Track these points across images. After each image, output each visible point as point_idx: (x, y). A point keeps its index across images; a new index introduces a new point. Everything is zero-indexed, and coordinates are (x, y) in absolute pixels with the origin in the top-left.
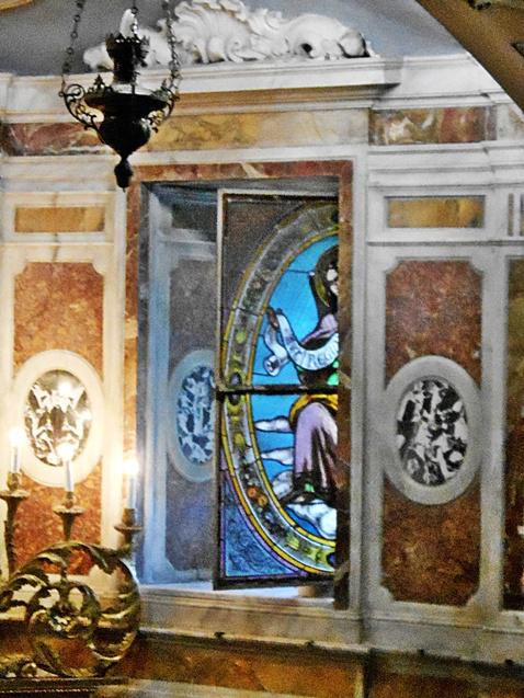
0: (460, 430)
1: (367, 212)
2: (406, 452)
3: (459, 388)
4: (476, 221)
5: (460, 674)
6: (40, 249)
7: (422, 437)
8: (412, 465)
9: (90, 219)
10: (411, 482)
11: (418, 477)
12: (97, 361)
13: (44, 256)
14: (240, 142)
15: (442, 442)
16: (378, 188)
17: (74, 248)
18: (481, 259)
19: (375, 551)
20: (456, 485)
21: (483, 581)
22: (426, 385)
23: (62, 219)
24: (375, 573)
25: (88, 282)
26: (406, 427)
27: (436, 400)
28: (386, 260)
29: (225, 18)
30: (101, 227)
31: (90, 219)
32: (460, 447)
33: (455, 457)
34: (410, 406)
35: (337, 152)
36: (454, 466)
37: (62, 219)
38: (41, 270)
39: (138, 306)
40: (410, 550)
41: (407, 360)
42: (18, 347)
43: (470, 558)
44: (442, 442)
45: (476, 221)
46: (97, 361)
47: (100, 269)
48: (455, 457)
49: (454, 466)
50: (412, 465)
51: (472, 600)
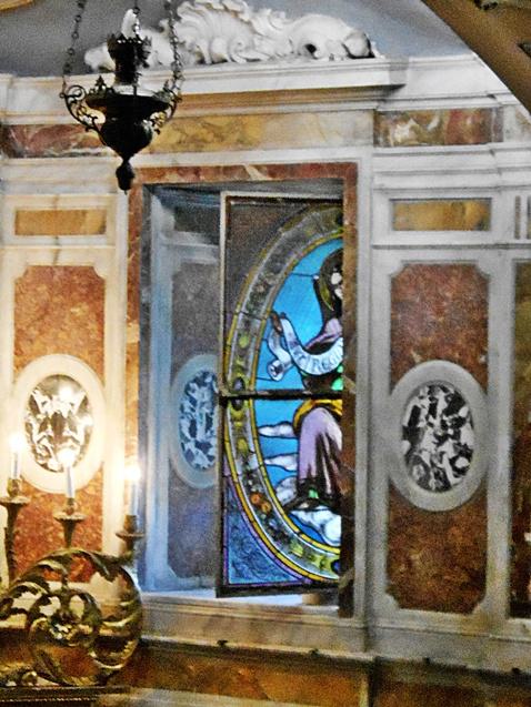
0: (466, 435)
1: (372, 215)
2: (411, 458)
3: (465, 393)
4: (482, 224)
5: (466, 683)
6: (40, 252)
7: (427, 442)
8: (418, 471)
9: (91, 221)
10: (417, 488)
11: (423, 483)
12: (98, 366)
13: (45, 260)
14: (244, 143)
15: (448, 448)
16: (383, 190)
17: (75, 251)
18: (488, 263)
19: (380, 558)
20: (462, 491)
21: (489, 588)
22: (432, 390)
23: (62, 222)
24: (380, 580)
25: (89, 286)
26: (411, 432)
27: (442, 405)
28: (391, 263)
29: (228, 18)
30: (102, 230)
31: (91, 221)
32: (466, 453)
33: (461, 463)
34: (416, 412)
35: (342, 154)
36: (460, 472)
37: (62, 222)
38: (42, 274)
39: (140, 310)
40: (416, 557)
41: (412, 364)
42: (18, 352)
43: (476, 566)
44: (448, 448)
45: (482, 224)
46: (98, 366)
47: (101, 272)
48: (461, 463)
49: (460, 472)
50: (418, 471)
51: (479, 608)
